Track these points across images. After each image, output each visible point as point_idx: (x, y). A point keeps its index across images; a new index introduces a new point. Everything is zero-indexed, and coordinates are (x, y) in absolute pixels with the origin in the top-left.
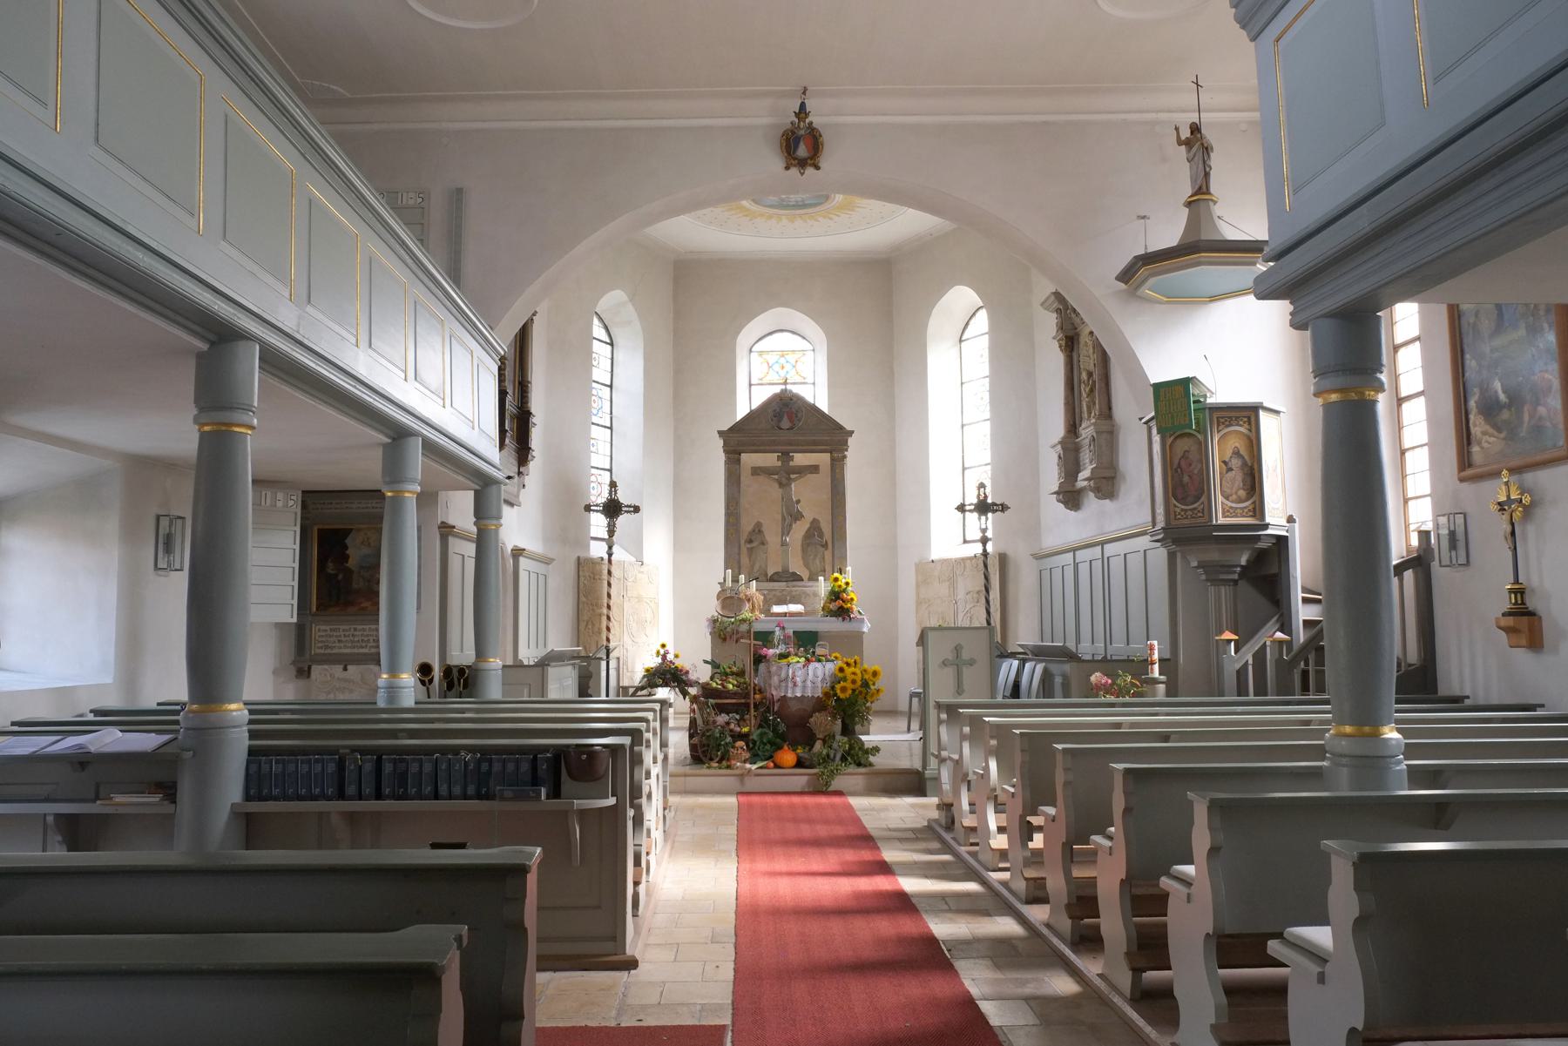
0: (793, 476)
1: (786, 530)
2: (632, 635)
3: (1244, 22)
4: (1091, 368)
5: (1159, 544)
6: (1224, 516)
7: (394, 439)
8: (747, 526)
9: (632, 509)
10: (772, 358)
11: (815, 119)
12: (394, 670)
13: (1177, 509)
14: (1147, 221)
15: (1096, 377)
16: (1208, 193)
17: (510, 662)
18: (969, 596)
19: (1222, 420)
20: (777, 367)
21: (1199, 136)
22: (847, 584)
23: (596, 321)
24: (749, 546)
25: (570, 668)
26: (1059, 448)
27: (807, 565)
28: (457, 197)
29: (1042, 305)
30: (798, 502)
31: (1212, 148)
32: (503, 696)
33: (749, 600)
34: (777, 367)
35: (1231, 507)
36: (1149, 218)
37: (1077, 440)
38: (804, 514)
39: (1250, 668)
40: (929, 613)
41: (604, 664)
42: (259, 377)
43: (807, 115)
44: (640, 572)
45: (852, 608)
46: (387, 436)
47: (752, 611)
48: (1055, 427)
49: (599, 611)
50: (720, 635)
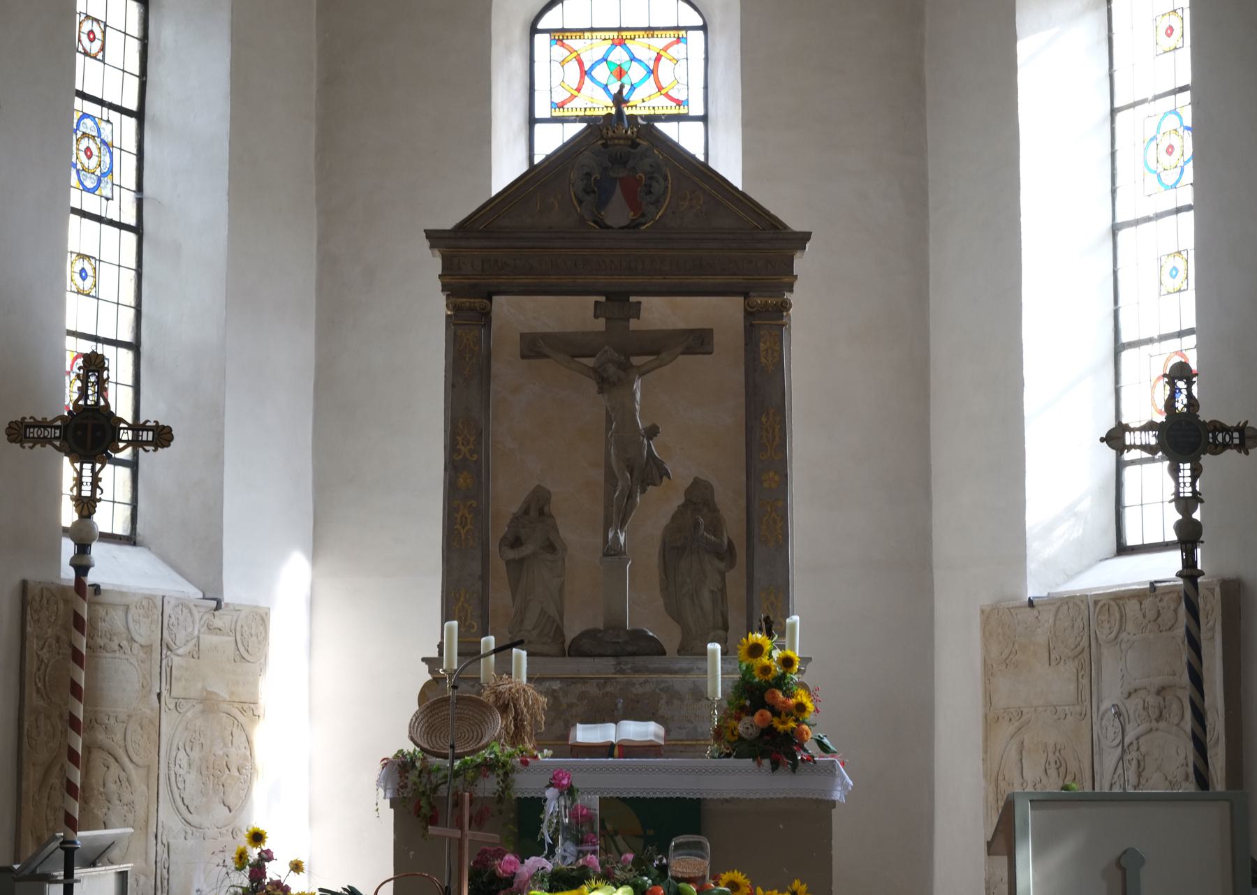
0: (636, 361)
1: (619, 513)
2: (184, 807)
10: (589, 50)
18: (1135, 703)
20: (602, 73)
22: (787, 662)
24: (512, 554)
27: (675, 613)
30: (652, 432)
33: (504, 709)
34: (602, 73)
38: (668, 466)
44: (211, 629)
45: (801, 734)
47: (516, 737)
49: (469, 762)
50: (418, 808)
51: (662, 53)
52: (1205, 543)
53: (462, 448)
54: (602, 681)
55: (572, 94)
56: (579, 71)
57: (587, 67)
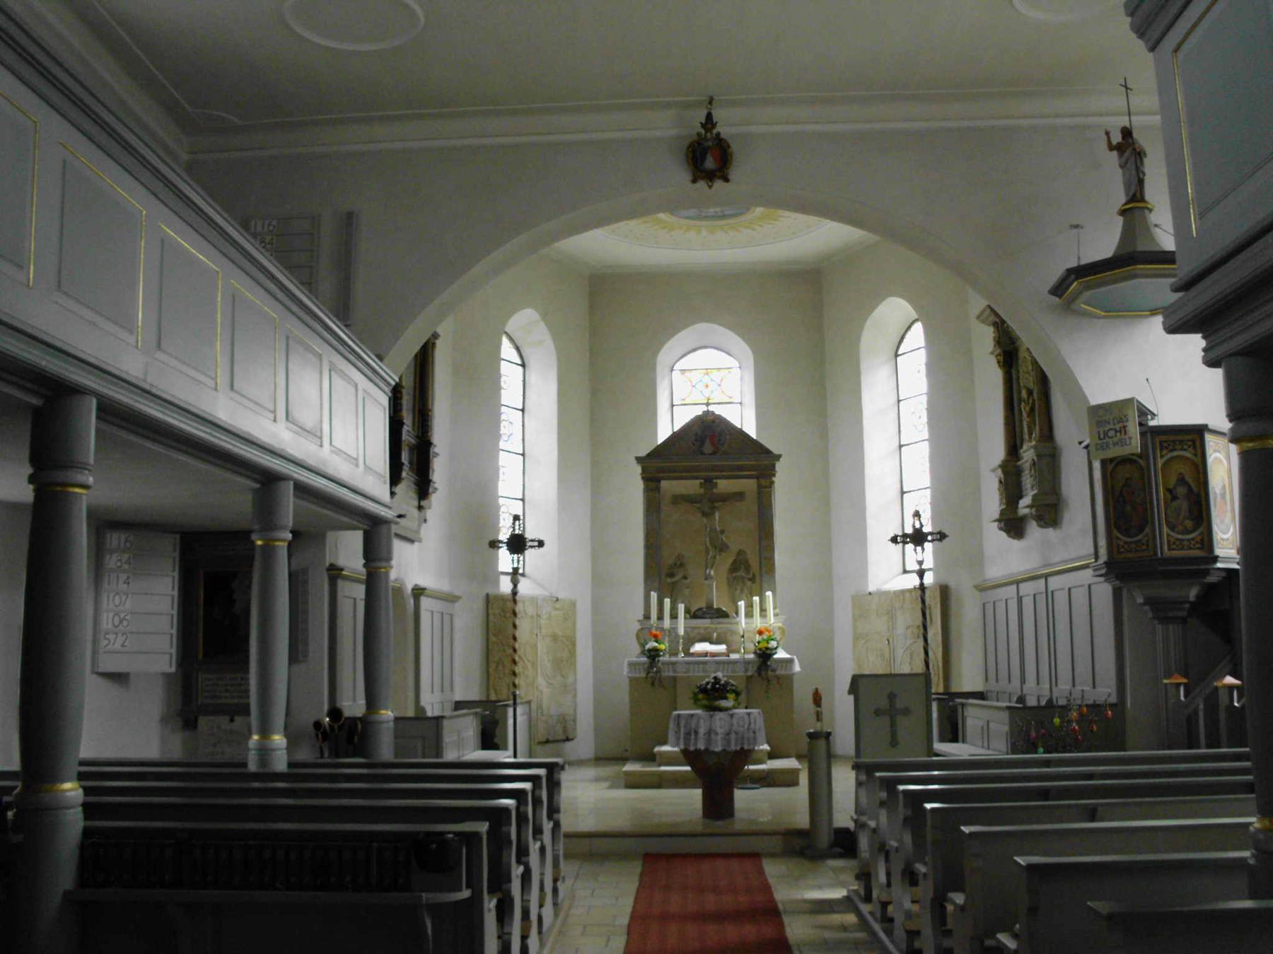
0: (716, 505)
3: (1141, 31)
4: (1031, 385)
5: (1102, 579)
6: (1169, 549)
7: (263, 484)
8: (668, 558)
9: (536, 544)
11: (723, 129)
12: (265, 731)
13: (1121, 543)
14: (1081, 230)
15: (1035, 395)
16: (1142, 200)
17: (410, 713)
19: (1166, 445)
21: (1130, 140)
23: (505, 340)
24: (669, 580)
25: (471, 717)
26: (999, 471)
28: (349, 221)
29: (978, 318)
30: (722, 532)
31: (1145, 154)
32: (396, 755)
35: (1177, 539)
36: (1082, 228)
37: (1019, 463)
39: (1201, 714)
40: (867, 648)
41: (510, 711)
42: (98, 431)
43: (714, 125)
46: (255, 480)
48: (995, 450)
52: (1147, 377)
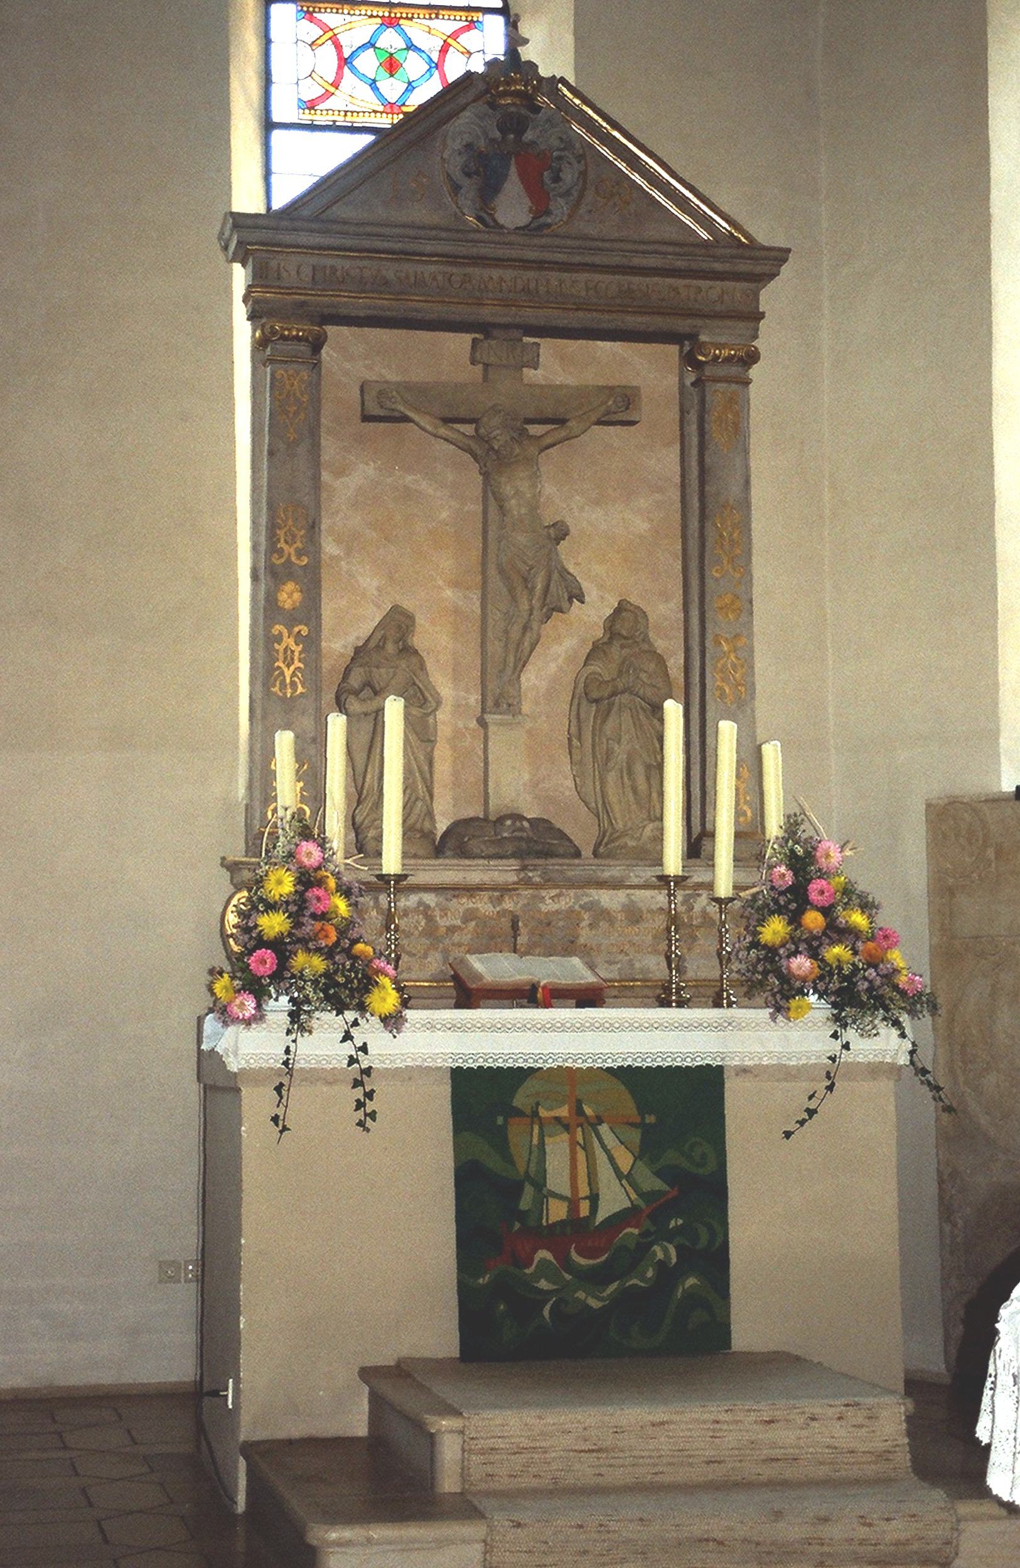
51: (450, 41)
53: (286, 547)
54: (496, 894)
55: (327, 90)
56: (336, 58)
57: (346, 53)
